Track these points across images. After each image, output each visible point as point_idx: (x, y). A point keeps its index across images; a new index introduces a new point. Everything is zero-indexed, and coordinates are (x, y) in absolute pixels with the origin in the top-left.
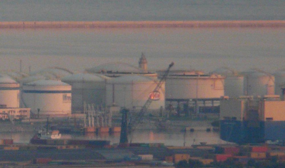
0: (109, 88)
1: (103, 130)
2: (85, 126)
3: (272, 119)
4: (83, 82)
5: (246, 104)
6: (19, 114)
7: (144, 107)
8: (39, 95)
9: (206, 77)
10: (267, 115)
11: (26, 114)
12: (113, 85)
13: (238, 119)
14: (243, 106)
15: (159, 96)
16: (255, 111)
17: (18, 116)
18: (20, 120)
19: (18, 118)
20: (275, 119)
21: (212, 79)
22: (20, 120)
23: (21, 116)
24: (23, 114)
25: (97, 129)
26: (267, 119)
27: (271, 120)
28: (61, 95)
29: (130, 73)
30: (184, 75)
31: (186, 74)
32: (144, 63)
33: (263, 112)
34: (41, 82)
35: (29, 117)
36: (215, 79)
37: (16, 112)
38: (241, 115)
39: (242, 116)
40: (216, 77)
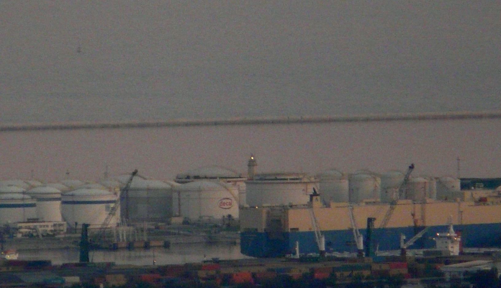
0: (175, 195)
1: (136, 245)
2: (116, 241)
3: (297, 229)
4: (149, 189)
5: (268, 213)
6: (53, 229)
7: (104, 224)
8: (77, 206)
9: (296, 180)
10: (291, 225)
11: (62, 228)
12: (179, 192)
13: (259, 231)
14: (264, 217)
15: (230, 204)
16: (277, 220)
17: (51, 231)
18: (54, 235)
19: (51, 233)
20: (301, 230)
21: (304, 183)
22: (54, 235)
23: (55, 230)
24: (57, 228)
25: (129, 244)
26: (291, 229)
27: (297, 232)
28: (103, 206)
29: (215, 178)
30: (276, 179)
31: (278, 178)
32: (254, 166)
33: (286, 221)
34: (82, 192)
35: (65, 231)
36: (306, 183)
37: (50, 226)
38: (262, 227)
39: (264, 227)
40: (309, 181)
